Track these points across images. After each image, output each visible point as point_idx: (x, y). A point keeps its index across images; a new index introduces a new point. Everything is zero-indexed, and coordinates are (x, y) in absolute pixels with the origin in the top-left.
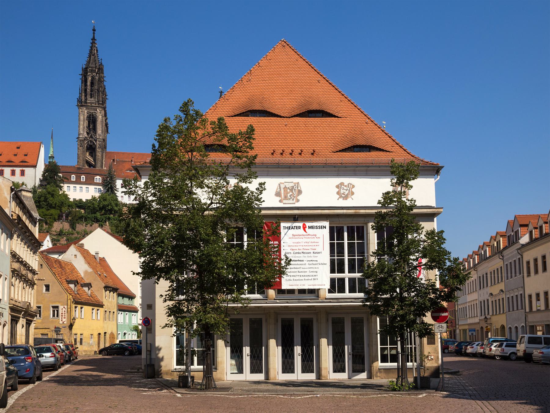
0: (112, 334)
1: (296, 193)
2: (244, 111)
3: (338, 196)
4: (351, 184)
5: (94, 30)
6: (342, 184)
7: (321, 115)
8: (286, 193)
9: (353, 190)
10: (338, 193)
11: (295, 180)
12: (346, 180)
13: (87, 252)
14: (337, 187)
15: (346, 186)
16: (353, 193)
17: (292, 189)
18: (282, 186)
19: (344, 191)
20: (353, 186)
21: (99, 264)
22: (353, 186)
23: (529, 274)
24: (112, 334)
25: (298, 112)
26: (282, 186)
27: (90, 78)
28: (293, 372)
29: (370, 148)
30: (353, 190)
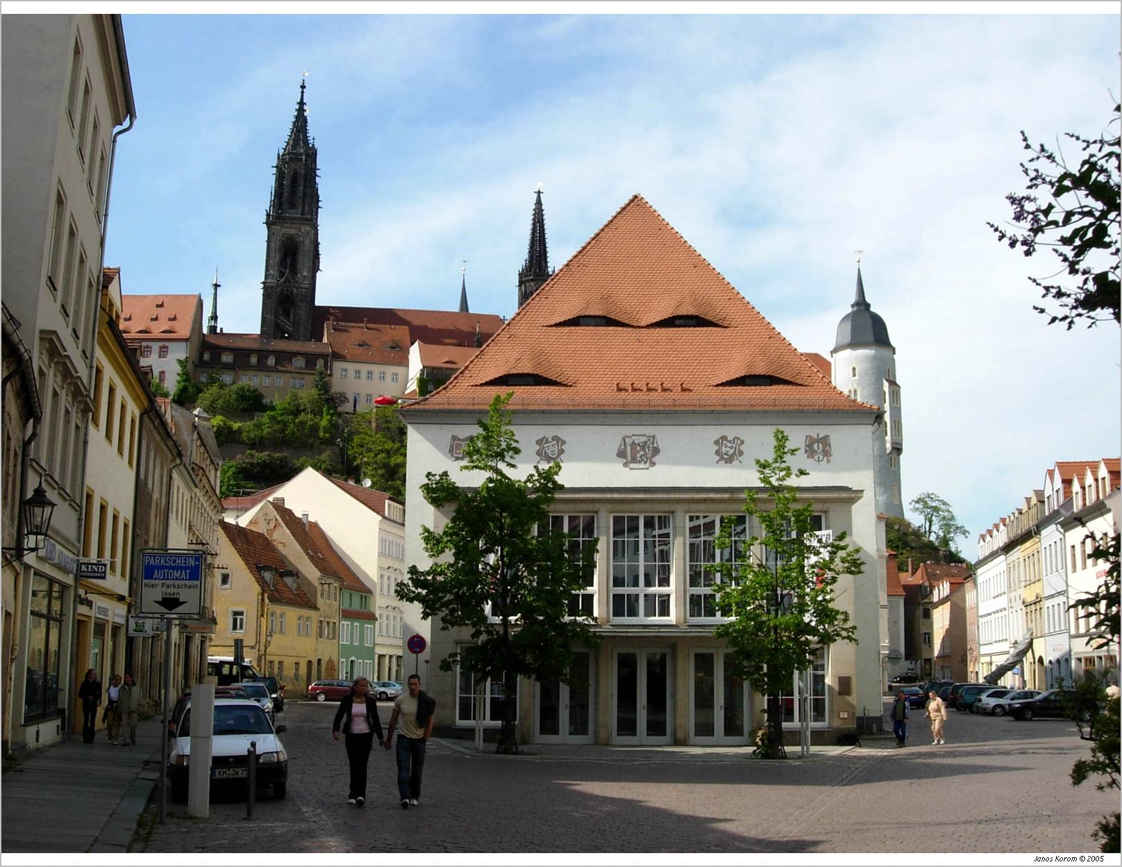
0: (330, 662)
1: (649, 453)
5: (303, 87)
6: (724, 438)
7: (693, 322)
8: (634, 452)
10: (717, 453)
11: (650, 430)
12: (731, 432)
13: (290, 512)
14: (716, 442)
16: (741, 453)
17: (643, 447)
18: (628, 441)
20: (742, 442)
21: (309, 535)
22: (742, 442)
23: (1074, 570)
24: (330, 662)
26: (628, 441)
28: (634, 734)
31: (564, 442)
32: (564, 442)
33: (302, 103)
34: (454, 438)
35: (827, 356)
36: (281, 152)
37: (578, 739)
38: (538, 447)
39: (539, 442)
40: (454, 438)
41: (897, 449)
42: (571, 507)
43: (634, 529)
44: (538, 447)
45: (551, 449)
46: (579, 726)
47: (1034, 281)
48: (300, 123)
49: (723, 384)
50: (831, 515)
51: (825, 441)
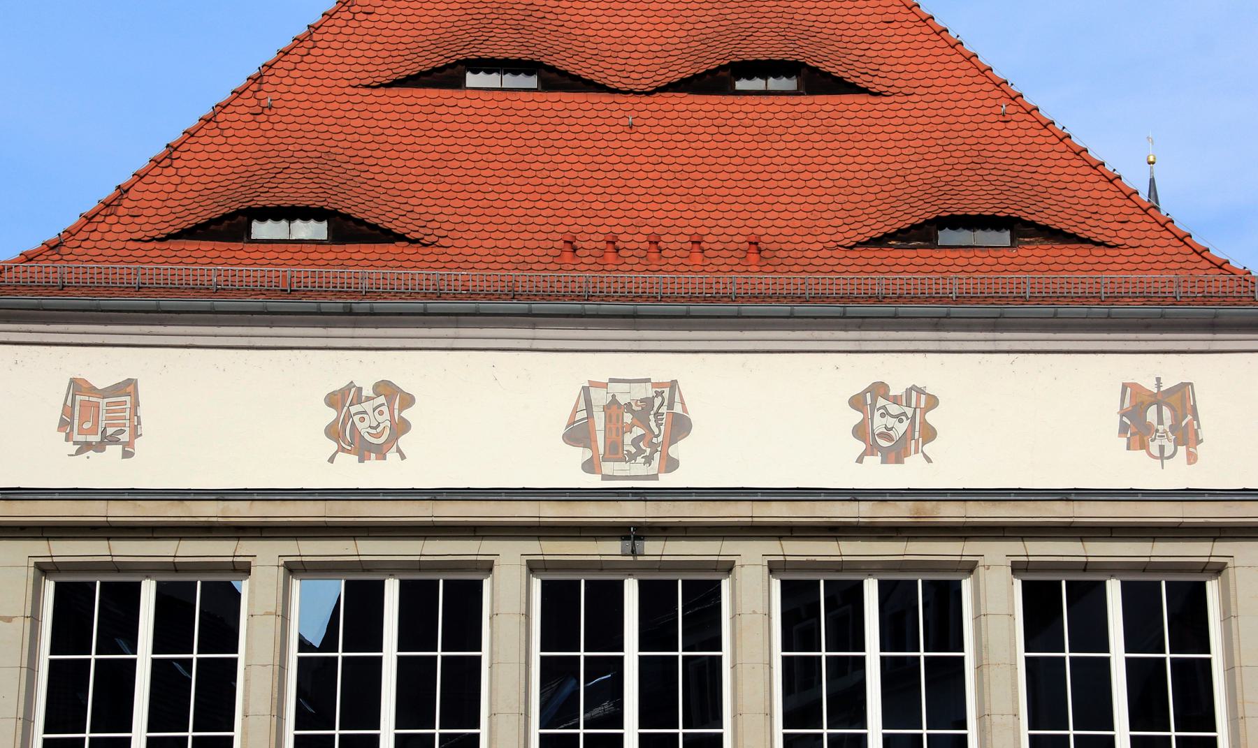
1: (660, 432)
3: (861, 446)
4: (920, 391)
6: (879, 389)
9: (931, 418)
10: (859, 431)
14: (856, 402)
15: (896, 400)
16: (929, 434)
17: (644, 410)
19: (891, 422)
20: (933, 402)
22: (933, 402)
30: (931, 418)
31: (408, 401)
32: (408, 401)
34: (77, 386)
38: (331, 414)
39: (334, 400)
40: (77, 386)
41: (139, 423)
43: (122, 630)
44: (331, 414)
45: (371, 420)
47: (556, 79)
51: (1180, 399)
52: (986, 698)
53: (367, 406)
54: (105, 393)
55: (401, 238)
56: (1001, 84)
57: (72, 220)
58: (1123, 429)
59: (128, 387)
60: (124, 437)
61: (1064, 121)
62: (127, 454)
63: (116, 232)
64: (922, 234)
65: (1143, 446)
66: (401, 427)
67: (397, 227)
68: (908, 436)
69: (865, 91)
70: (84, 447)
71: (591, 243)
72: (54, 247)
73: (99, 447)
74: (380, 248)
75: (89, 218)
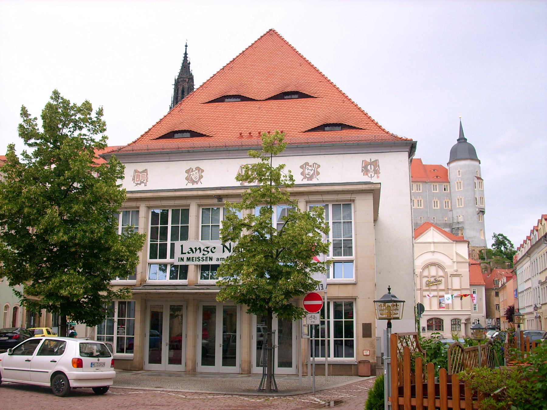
2: (219, 97)
3: (303, 177)
4: (316, 164)
5: (186, 46)
6: (307, 164)
7: (296, 96)
9: (319, 170)
10: (302, 174)
14: (302, 167)
15: (311, 166)
16: (318, 174)
19: (309, 171)
20: (319, 166)
22: (319, 166)
25: (273, 95)
27: (181, 88)
29: (343, 126)
30: (319, 170)
31: (203, 171)
32: (203, 171)
33: (186, 54)
34: (136, 171)
35: (446, 167)
36: (176, 78)
37: (175, 368)
39: (187, 172)
40: (136, 171)
42: (172, 203)
45: (195, 175)
46: (175, 360)
48: (186, 65)
49: (309, 131)
50: (357, 202)
51: (375, 163)
52: (232, 100)
53: (194, 173)
54: (141, 173)
55: (205, 135)
56: (343, 94)
57: (139, 136)
58: (362, 171)
59: (145, 171)
60: (145, 182)
61: (356, 101)
62: (145, 185)
63: (148, 138)
64: (321, 128)
65: (367, 175)
66: (201, 177)
67: (204, 133)
68: (314, 174)
69: (313, 97)
70: (137, 184)
71: (246, 134)
72: (134, 142)
73: (140, 184)
74: (200, 138)
75: (142, 136)
